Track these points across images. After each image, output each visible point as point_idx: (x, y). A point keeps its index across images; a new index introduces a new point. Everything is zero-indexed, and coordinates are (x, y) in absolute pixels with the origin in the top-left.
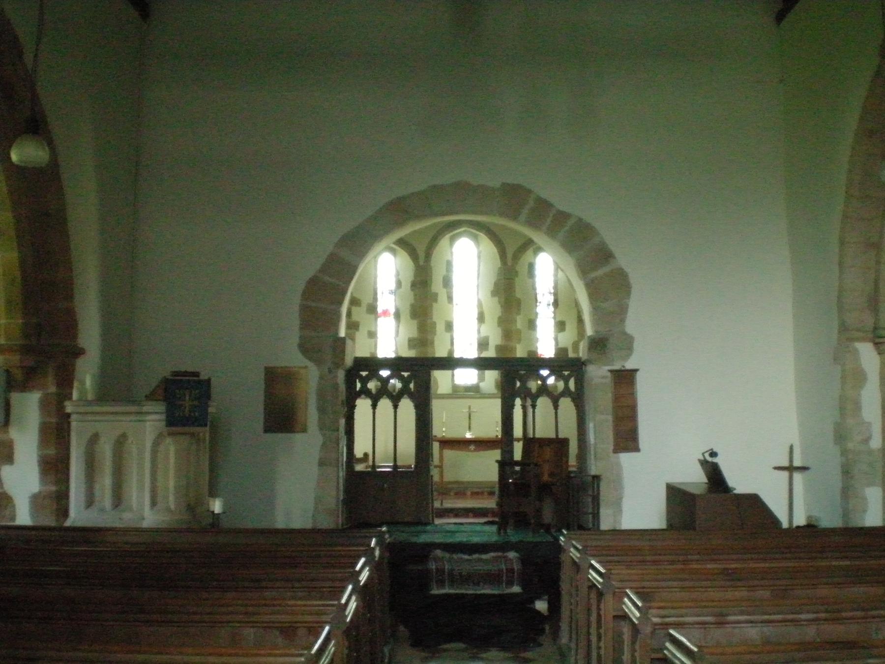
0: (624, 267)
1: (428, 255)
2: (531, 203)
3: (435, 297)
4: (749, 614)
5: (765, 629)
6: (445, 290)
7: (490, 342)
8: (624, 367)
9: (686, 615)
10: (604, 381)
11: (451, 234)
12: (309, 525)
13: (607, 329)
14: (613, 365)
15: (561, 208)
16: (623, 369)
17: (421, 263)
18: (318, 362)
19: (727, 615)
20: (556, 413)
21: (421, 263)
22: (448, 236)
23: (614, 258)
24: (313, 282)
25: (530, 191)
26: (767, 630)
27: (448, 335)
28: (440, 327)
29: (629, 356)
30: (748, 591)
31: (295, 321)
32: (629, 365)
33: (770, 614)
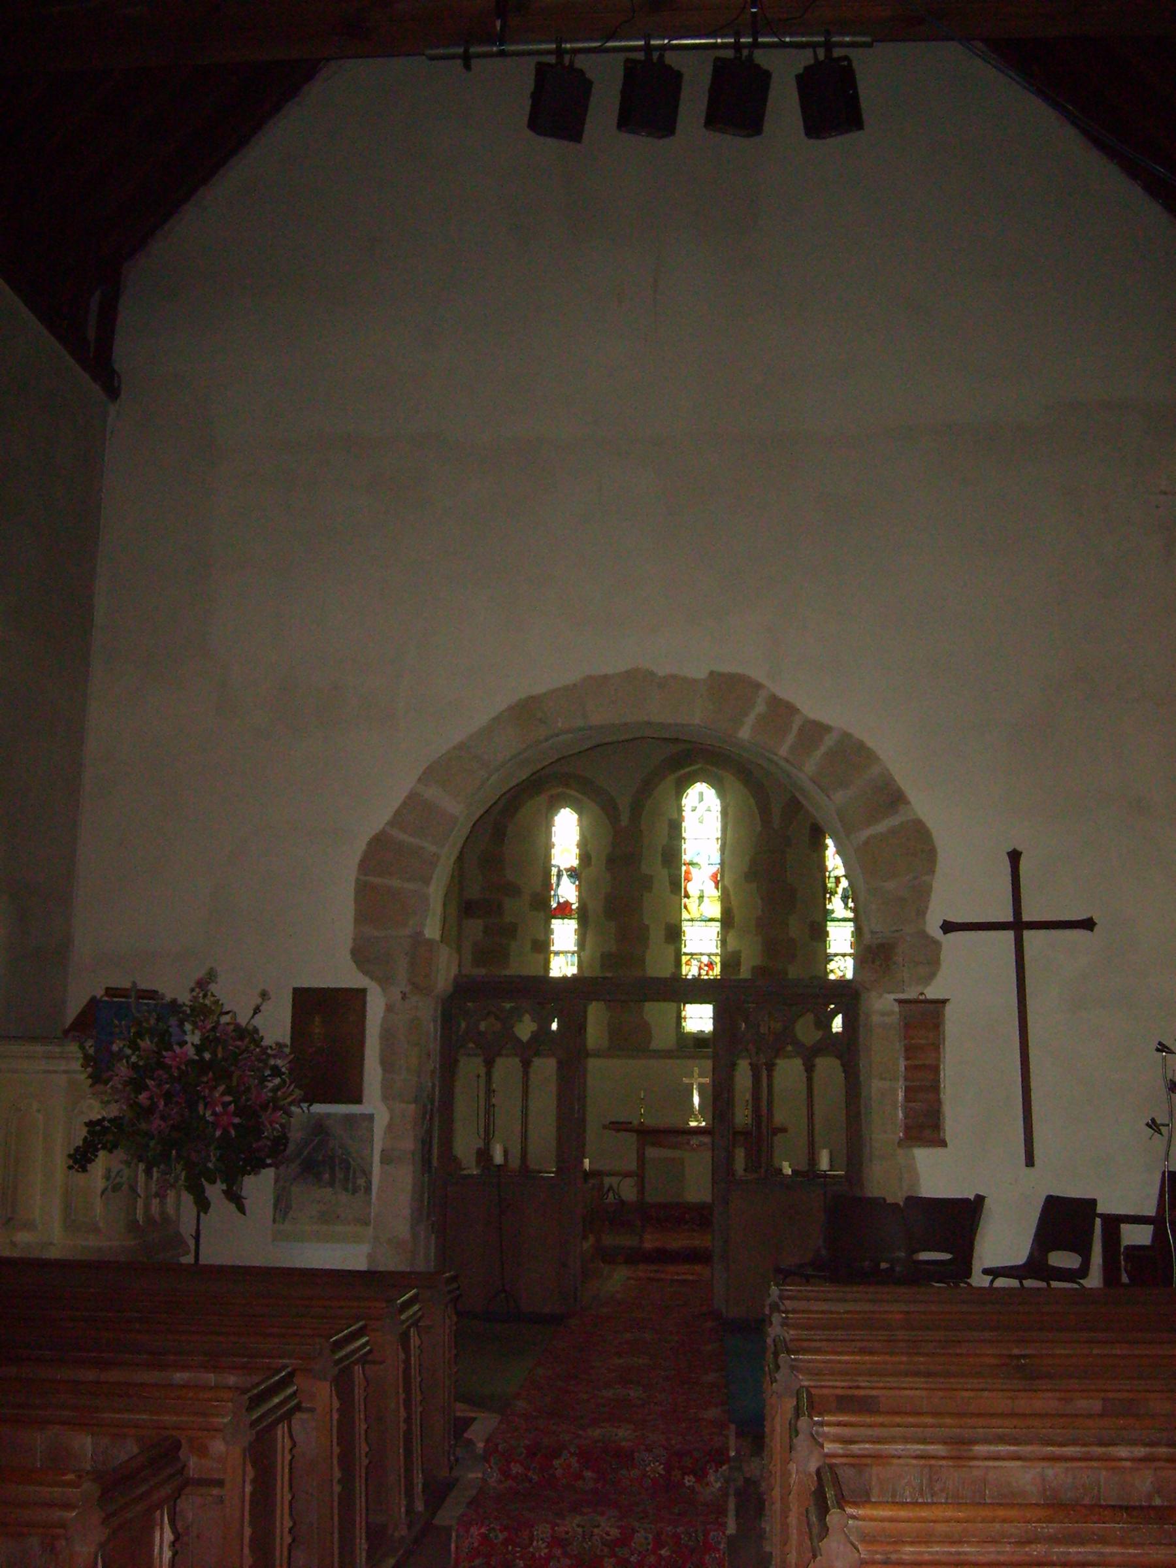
0: (924, 819)
1: (637, 810)
2: (760, 707)
3: (646, 883)
4: (1015, 1442)
5: (1050, 1472)
6: (665, 872)
7: (742, 960)
8: (922, 994)
9: (892, 1440)
10: (887, 1019)
11: (678, 774)
12: (366, 1269)
13: (894, 928)
14: (903, 992)
15: (812, 715)
16: (921, 997)
17: (625, 821)
18: (385, 981)
19: (973, 1442)
20: (810, 1079)
21: (625, 821)
22: (672, 778)
23: (908, 803)
24: (379, 843)
25: (758, 686)
26: (1052, 1472)
27: (671, 949)
28: (656, 935)
29: (932, 976)
30: (1059, 1399)
31: (347, 909)
32: (932, 993)
33: (1061, 1445)
